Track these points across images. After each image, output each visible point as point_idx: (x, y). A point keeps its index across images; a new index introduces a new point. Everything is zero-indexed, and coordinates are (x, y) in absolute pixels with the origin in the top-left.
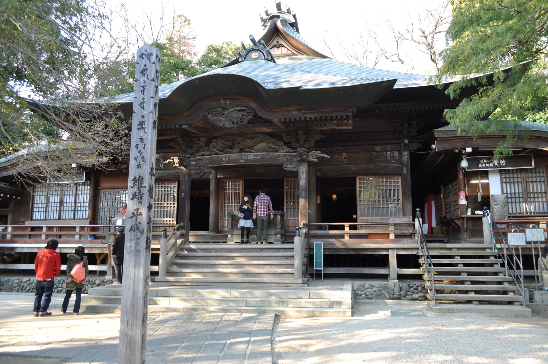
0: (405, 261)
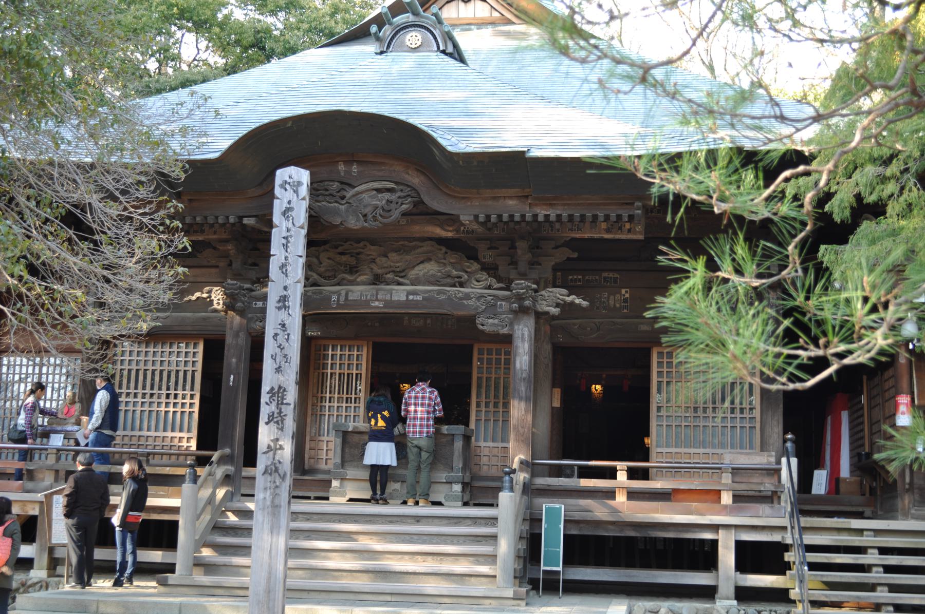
0: (755, 557)
